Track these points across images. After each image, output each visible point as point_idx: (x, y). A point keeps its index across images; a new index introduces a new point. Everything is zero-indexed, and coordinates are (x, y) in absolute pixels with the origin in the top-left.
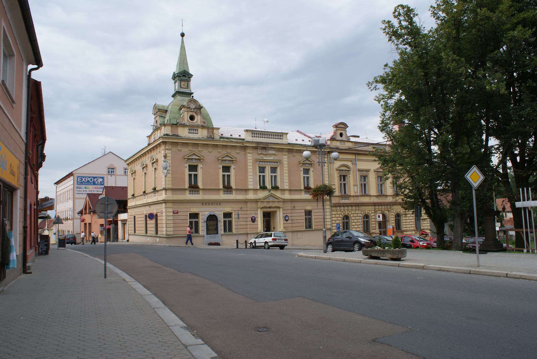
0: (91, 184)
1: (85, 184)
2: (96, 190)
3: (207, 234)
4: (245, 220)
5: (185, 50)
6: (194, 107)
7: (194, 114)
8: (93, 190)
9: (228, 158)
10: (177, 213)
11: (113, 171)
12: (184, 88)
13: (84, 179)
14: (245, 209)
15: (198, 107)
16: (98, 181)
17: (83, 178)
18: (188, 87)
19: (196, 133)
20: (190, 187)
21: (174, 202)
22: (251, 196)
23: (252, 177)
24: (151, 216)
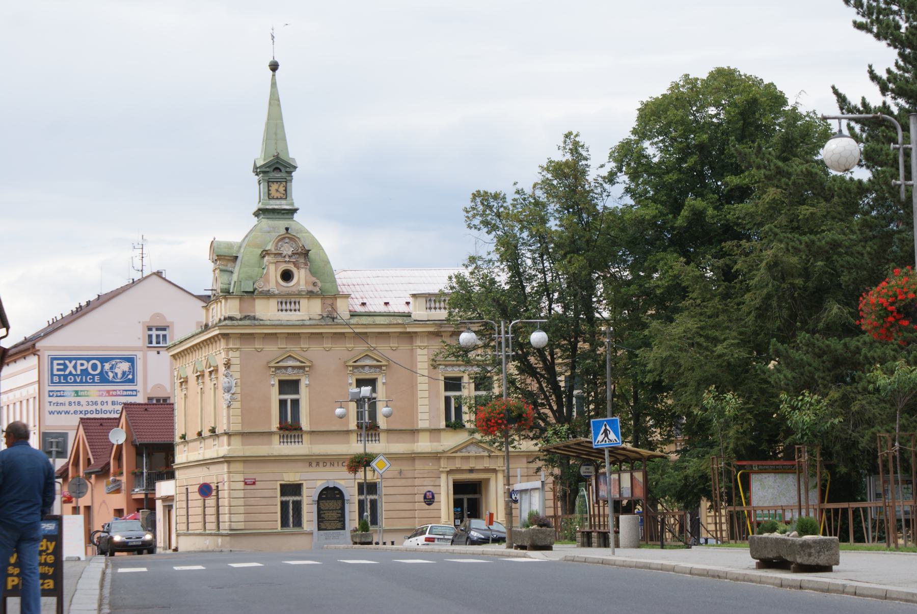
0: (94, 382)
1: (75, 382)
2: (110, 399)
3: (319, 529)
4: (409, 498)
5: (279, 105)
6: (290, 253)
7: (291, 267)
8: (99, 400)
9: (368, 362)
10: (254, 483)
11: (164, 336)
12: (277, 198)
13: (70, 368)
14: (409, 475)
15: (300, 250)
16: (117, 370)
17: (67, 362)
18: (286, 195)
19: (295, 310)
20: (281, 428)
21: (246, 460)
22: (424, 445)
23: (426, 401)
24: (205, 490)
